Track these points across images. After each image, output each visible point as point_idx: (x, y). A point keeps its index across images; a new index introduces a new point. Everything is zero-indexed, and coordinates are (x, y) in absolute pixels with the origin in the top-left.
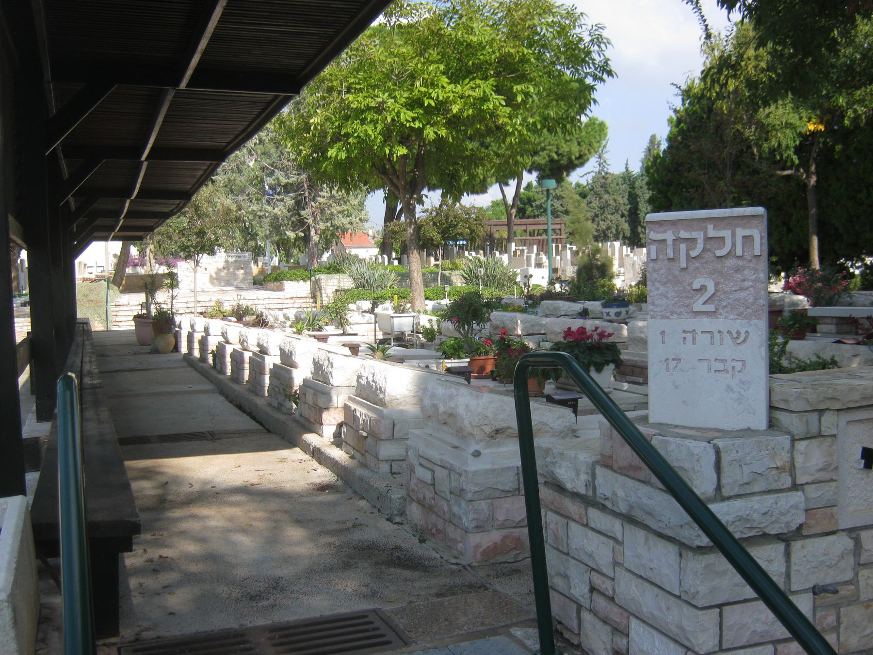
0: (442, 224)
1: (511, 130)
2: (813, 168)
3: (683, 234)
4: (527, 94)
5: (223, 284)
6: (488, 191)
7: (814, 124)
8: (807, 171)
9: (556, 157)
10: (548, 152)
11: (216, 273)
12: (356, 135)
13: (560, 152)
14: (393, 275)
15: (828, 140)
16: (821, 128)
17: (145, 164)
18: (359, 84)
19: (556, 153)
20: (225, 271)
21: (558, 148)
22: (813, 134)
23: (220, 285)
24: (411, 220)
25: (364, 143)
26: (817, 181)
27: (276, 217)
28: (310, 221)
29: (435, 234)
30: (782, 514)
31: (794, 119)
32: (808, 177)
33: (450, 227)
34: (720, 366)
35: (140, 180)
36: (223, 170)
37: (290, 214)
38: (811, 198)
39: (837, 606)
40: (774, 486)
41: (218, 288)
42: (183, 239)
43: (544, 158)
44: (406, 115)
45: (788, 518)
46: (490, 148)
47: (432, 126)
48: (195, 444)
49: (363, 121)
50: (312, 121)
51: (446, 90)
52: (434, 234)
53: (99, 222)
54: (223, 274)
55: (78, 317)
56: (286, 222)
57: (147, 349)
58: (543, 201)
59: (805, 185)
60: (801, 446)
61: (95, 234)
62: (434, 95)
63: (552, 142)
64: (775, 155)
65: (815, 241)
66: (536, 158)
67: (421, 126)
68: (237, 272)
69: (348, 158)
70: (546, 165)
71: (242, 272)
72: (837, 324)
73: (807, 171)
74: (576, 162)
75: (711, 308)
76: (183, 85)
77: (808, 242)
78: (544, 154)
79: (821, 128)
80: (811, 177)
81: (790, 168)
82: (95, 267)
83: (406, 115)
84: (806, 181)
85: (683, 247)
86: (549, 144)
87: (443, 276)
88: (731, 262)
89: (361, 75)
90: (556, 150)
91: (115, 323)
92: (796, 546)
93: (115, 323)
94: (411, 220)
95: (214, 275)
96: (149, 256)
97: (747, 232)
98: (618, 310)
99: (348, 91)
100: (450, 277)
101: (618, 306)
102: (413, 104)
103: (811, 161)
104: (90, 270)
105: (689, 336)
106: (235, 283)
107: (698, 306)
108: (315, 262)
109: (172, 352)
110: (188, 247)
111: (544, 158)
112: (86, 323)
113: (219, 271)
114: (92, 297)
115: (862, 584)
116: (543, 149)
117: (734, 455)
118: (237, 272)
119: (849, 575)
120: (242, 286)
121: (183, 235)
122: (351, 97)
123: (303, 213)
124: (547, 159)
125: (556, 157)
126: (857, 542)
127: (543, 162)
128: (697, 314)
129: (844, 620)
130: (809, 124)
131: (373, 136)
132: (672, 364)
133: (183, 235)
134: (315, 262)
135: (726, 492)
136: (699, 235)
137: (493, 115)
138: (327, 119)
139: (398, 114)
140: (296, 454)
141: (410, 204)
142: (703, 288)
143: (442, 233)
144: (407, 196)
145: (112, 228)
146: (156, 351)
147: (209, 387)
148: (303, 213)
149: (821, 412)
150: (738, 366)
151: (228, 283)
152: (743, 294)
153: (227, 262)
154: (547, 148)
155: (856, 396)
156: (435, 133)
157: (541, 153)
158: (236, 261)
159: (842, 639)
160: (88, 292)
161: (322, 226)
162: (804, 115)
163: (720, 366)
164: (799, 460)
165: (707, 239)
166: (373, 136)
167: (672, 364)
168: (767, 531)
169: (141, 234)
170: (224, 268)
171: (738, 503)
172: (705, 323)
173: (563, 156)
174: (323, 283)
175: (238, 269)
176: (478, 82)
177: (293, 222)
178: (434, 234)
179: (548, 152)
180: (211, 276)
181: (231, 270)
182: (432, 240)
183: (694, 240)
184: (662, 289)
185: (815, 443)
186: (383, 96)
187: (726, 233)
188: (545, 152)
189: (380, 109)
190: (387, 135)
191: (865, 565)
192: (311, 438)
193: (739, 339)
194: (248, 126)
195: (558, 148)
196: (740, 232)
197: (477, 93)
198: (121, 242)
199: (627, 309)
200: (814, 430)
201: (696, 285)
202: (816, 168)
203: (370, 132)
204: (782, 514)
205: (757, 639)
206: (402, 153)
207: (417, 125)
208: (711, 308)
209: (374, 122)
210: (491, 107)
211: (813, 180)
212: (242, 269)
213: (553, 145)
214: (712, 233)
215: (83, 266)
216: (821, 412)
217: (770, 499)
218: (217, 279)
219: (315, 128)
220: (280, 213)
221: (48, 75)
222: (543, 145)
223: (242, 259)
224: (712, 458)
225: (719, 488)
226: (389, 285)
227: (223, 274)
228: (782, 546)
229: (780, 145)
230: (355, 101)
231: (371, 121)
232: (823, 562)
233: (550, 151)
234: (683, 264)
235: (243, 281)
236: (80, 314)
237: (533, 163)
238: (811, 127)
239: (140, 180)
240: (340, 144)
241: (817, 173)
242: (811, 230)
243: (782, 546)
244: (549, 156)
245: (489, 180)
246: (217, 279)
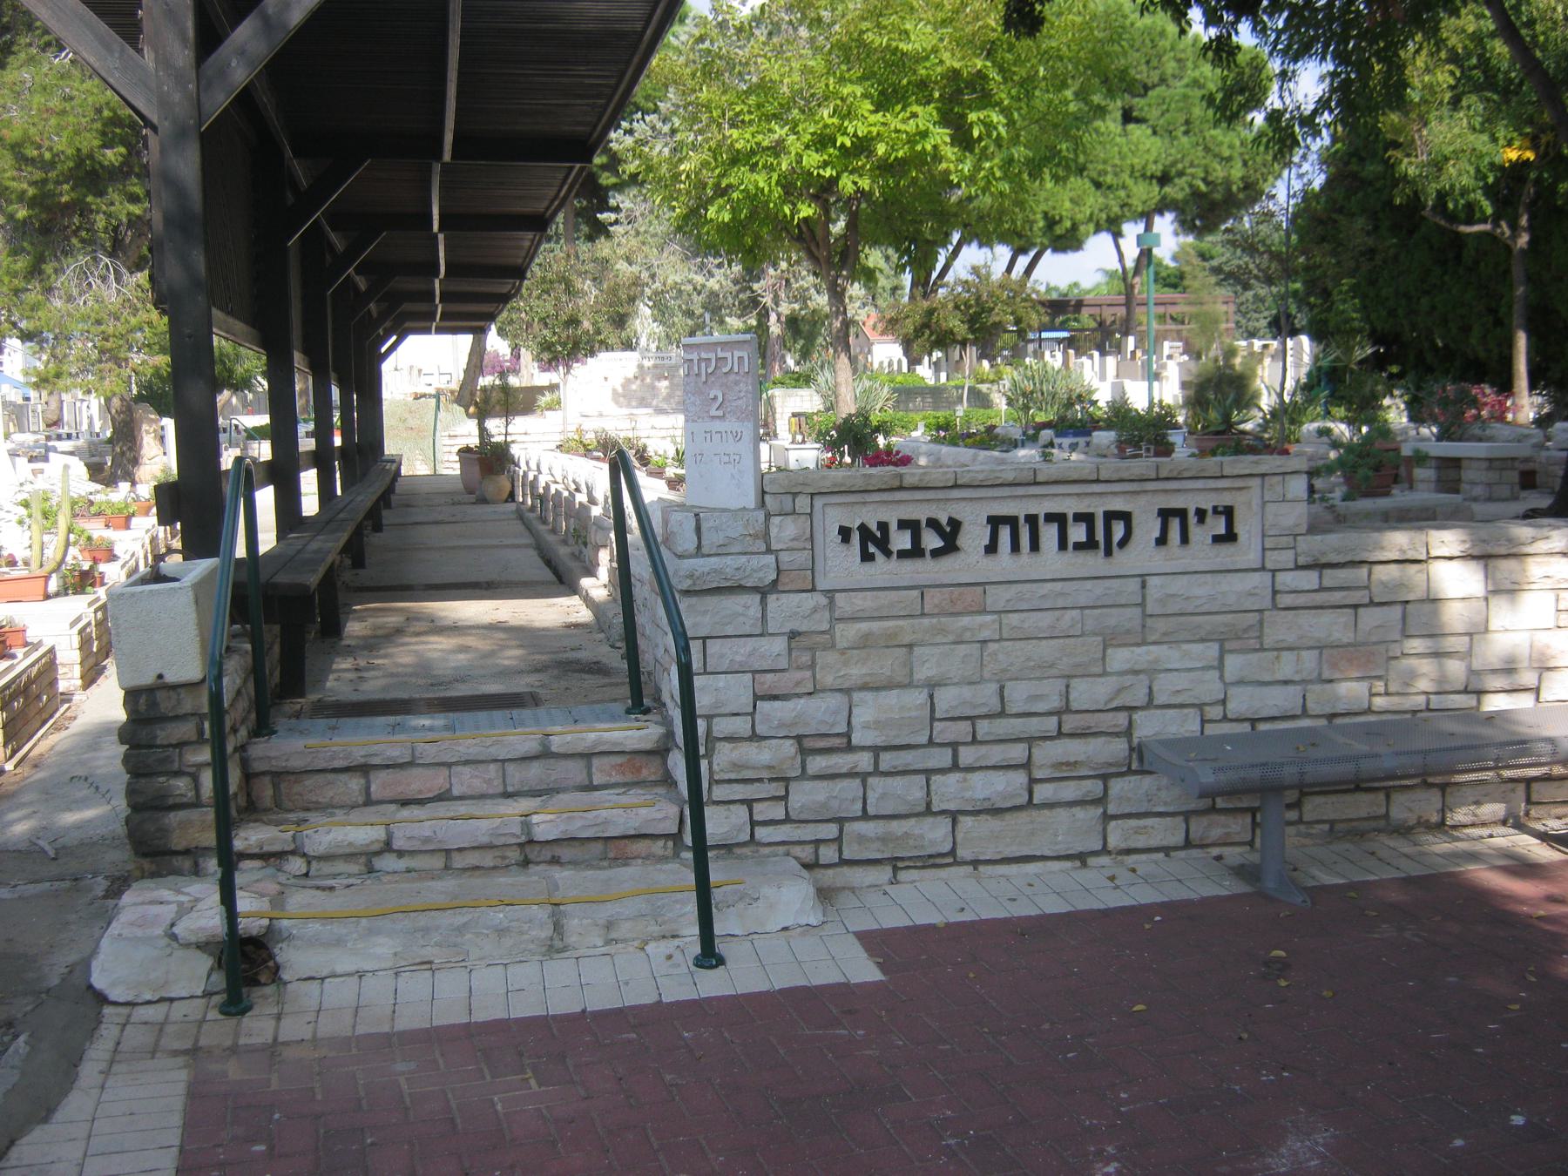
0: (968, 307)
1: (956, 181)
2: (1524, 221)
3: (704, 355)
4: (988, 126)
5: (634, 404)
6: (1085, 247)
7: (1520, 148)
8: (1514, 227)
9: (1203, 187)
10: (1189, 178)
11: (623, 386)
12: (742, 187)
13: (1210, 178)
14: (886, 390)
15: (1546, 175)
16: (1530, 155)
17: (441, 237)
18: (750, 112)
19: (1204, 180)
20: (638, 382)
21: (1207, 172)
22: (1522, 165)
23: (629, 406)
24: (838, 309)
25: (754, 198)
26: (1530, 243)
27: (714, 294)
28: (767, 300)
29: (957, 323)
30: (755, 571)
31: (1481, 142)
32: (1514, 236)
33: (983, 312)
34: (726, 459)
35: (442, 254)
36: (627, 218)
37: (737, 287)
38: (1517, 271)
39: (812, 649)
40: (750, 550)
41: (625, 411)
42: (545, 332)
43: (1182, 189)
44: (812, 159)
45: (761, 574)
46: (1085, 174)
47: (851, 173)
48: (463, 592)
49: (753, 168)
50: (682, 167)
51: (867, 121)
52: (957, 325)
53: (407, 307)
54: (634, 387)
55: (387, 452)
56: (730, 300)
57: (472, 498)
58: (1224, 259)
59: (1508, 249)
60: (776, 520)
61: (407, 324)
62: (851, 130)
63: (1196, 162)
64: (1446, 203)
65: (1521, 341)
66: (1167, 189)
67: (834, 174)
68: (657, 383)
69: (733, 219)
70: (1185, 201)
71: (665, 383)
72: (1438, 468)
73: (1514, 227)
74: (1241, 196)
75: (720, 413)
76: (447, 157)
77: (1510, 344)
78: (1182, 182)
79: (1530, 155)
80: (1520, 236)
81: (1485, 221)
82: (437, 374)
83: (812, 159)
84: (1509, 242)
85: (703, 365)
86: (1192, 165)
87: (973, 391)
88: (732, 377)
89: (752, 100)
90: (1202, 175)
91: (447, 465)
92: (771, 598)
93: (447, 465)
94: (838, 309)
95: (620, 390)
96: (526, 356)
97: (741, 354)
98: (1075, 440)
99: (733, 125)
100: (988, 395)
101: (1075, 435)
102: (822, 141)
103: (1521, 210)
104: (428, 379)
105: (708, 436)
106: (654, 403)
107: (713, 412)
108: (777, 367)
109: (506, 501)
110: (553, 344)
111: (1182, 189)
112: (397, 462)
113: (628, 381)
114: (412, 423)
115: (838, 635)
116: (1181, 174)
117: (711, 524)
118: (657, 383)
119: (825, 626)
120: (665, 406)
121: (546, 325)
122: (735, 133)
123: (756, 286)
124: (1188, 190)
125: (1203, 187)
126: (832, 601)
127: (1180, 196)
128: (713, 417)
129: (819, 661)
130: (1508, 150)
131: (766, 190)
132: (699, 458)
133: (546, 325)
134: (777, 367)
135: (705, 550)
136: (712, 356)
137: (937, 156)
138: (705, 164)
139: (799, 157)
140: (575, 600)
141: (837, 285)
142: (715, 398)
143: (969, 321)
144: (833, 273)
145: (430, 316)
146: (483, 500)
147: (528, 540)
148: (756, 286)
149: (795, 495)
150: (737, 458)
151: (643, 403)
152: (740, 402)
153: (641, 367)
154: (1189, 171)
155: (828, 483)
156: (855, 183)
157: (1177, 180)
158: (655, 366)
159: (818, 676)
160: (407, 415)
161: (785, 309)
162: (1501, 134)
163: (726, 459)
164: (774, 531)
165: (718, 359)
166: (766, 190)
167: (699, 458)
168: (742, 583)
169: (481, 324)
170: (636, 378)
171: (713, 560)
172: (718, 426)
173: (1216, 185)
174: (778, 403)
175: (659, 380)
176: (916, 108)
177: (740, 303)
178: (957, 325)
179: (1189, 178)
180: (615, 391)
181: (648, 380)
182: (952, 332)
183: (709, 359)
184: (692, 399)
185: (789, 518)
186: (780, 131)
187: (728, 355)
188: (1184, 179)
189: (778, 149)
190: (789, 188)
191: (839, 620)
192: (586, 582)
193: (738, 437)
194: (559, 191)
195: (1207, 172)
196: (737, 354)
197: (911, 127)
198: (471, 336)
199: (1088, 439)
200: (789, 508)
201: (712, 396)
202: (1529, 220)
203: (761, 184)
204: (755, 571)
205: (736, 668)
206: (806, 215)
207: (828, 172)
208: (720, 413)
209: (770, 168)
210: (929, 148)
211: (1523, 240)
212: (666, 378)
213: (1198, 166)
214: (720, 355)
215: (415, 372)
216: (795, 495)
217: (743, 559)
218: (624, 396)
219: (688, 176)
220: (717, 287)
221: (289, 153)
222: (1180, 166)
223: (666, 362)
224: (693, 524)
225: (699, 546)
226: (878, 407)
227: (634, 387)
228: (758, 597)
229: (1452, 186)
230: (740, 139)
231: (765, 167)
232: (796, 613)
233: (1193, 176)
234: (704, 379)
235: (668, 398)
236: (390, 448)
237: (1164, 198)
238: (1513, 155)
239: (442, 254)
240: (720, 201)
241: (1531, 228)
242: (1515, 323)
243: (758, 597)
244: (1191, 186)
245: (1082, 228)
246: (624, 396)
